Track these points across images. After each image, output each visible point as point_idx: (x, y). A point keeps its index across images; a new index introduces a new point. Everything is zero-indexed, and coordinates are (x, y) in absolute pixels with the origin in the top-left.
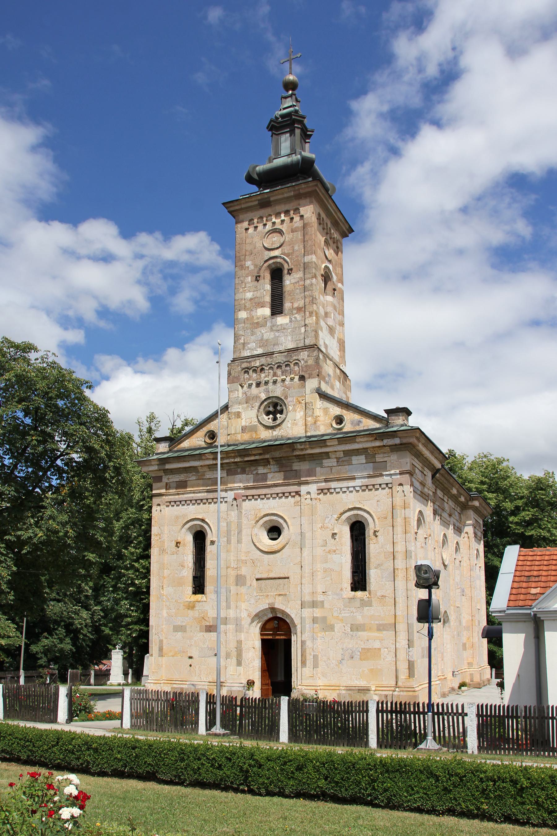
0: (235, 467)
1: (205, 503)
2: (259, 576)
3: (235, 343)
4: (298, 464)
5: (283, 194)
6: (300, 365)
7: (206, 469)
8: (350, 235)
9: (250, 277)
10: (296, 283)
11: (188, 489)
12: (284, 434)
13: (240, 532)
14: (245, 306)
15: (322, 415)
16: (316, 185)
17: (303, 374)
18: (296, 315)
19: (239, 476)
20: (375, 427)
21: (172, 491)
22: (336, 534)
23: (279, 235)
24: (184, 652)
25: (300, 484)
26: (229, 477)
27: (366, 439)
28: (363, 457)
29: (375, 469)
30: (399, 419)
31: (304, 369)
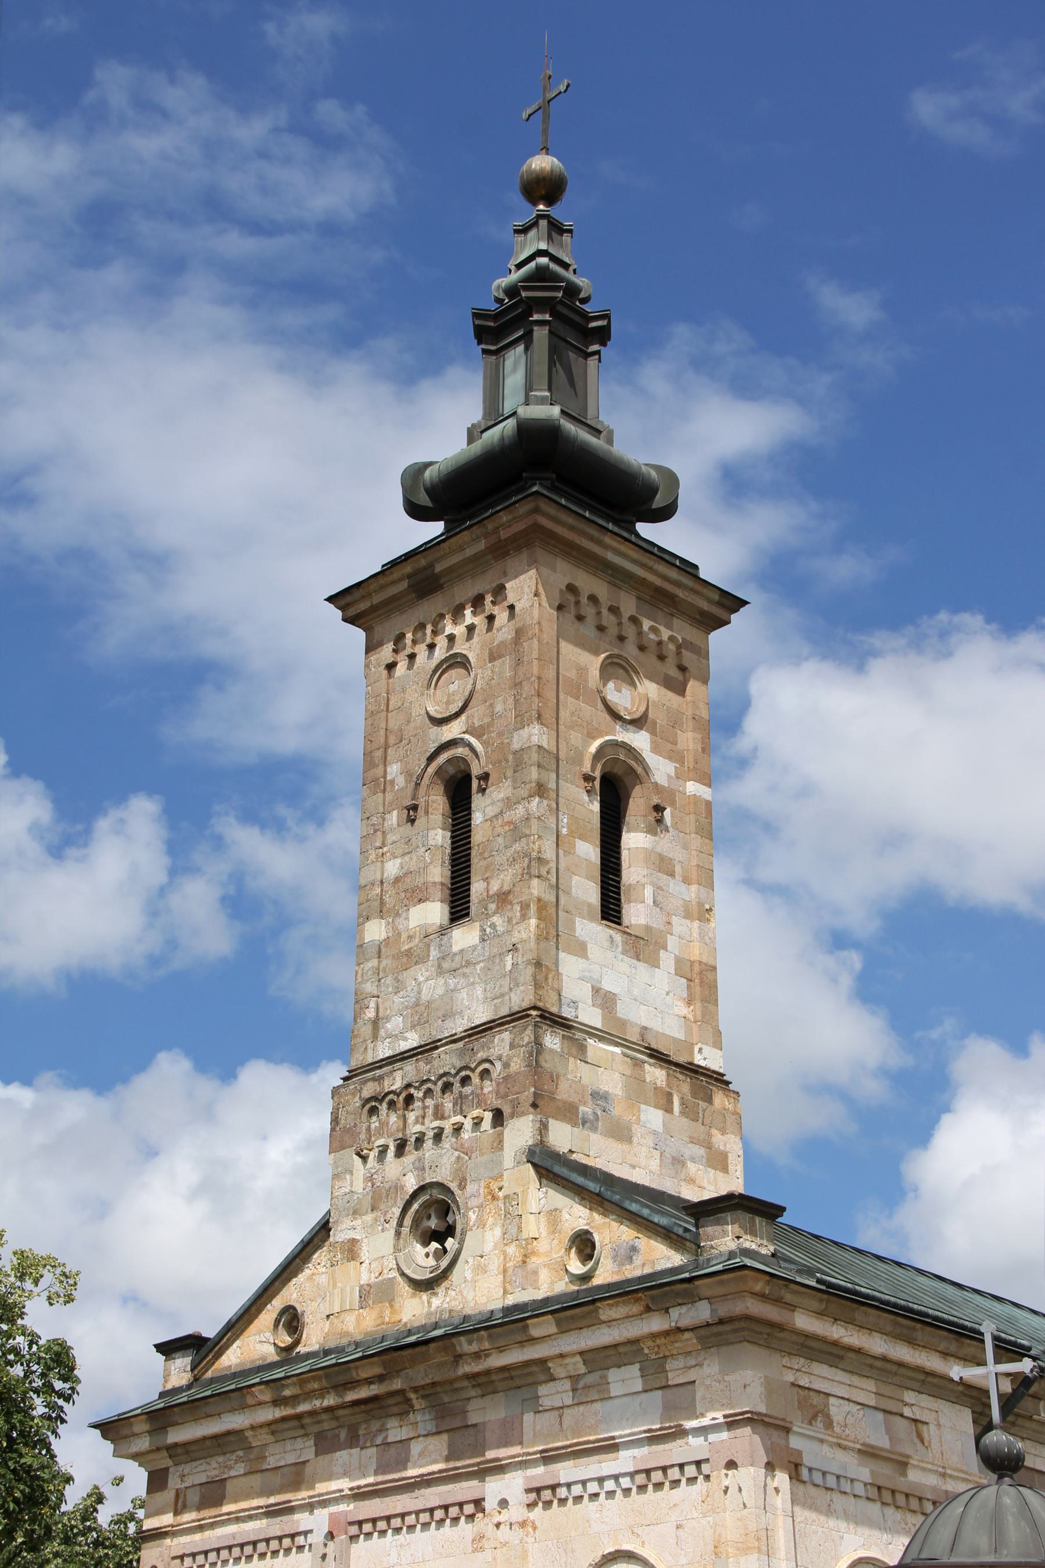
0: (334, 1424)
5: (461, 549)
7: (264, 1437)
8: (734, 617)
11: (226, 1509)
12: (456, 1305)
15: (544, 1233)
16: (536, 510)
18: (496, 919)
19: (343, 1456)
20: (669, 1265)
21: (189, 1517)
23: (462, 671)
25: (483, 1473)
28: (634, 1370)
29: (669, 1409)
30: (725, 1234)
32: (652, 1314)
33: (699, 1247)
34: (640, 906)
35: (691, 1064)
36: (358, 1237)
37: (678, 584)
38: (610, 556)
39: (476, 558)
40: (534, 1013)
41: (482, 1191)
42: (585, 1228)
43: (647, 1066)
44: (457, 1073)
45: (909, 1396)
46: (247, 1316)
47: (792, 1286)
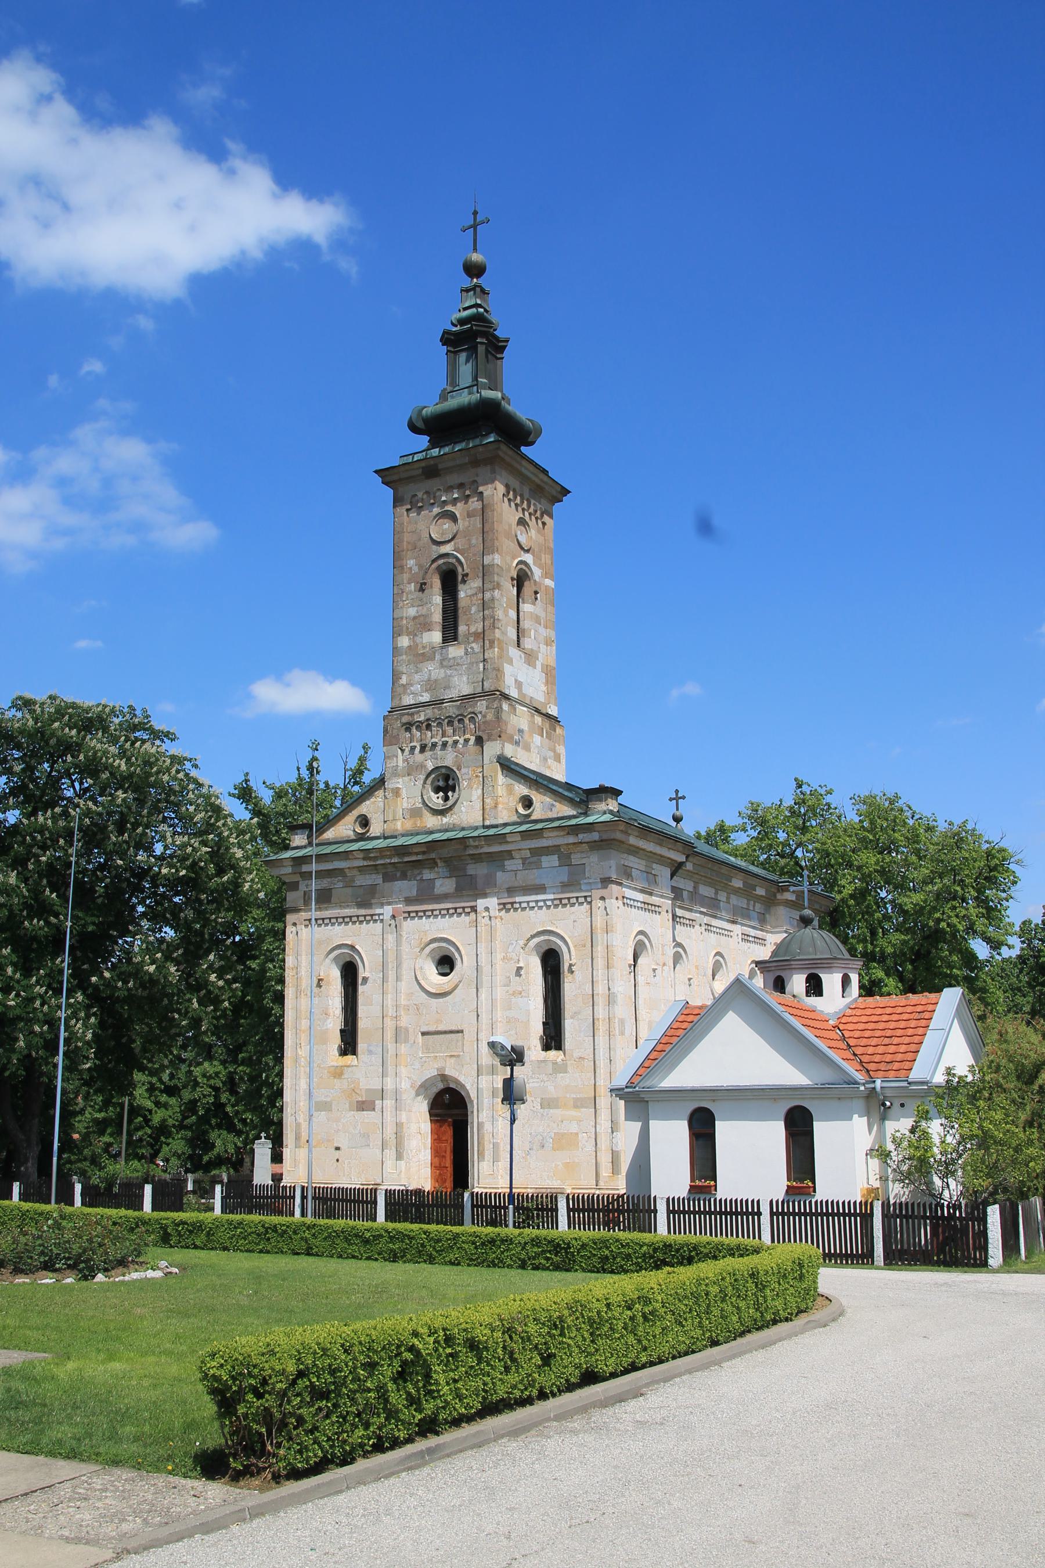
1: (354, 923)
2: (425, 1029)
4: (473, 866)
7: (355, 872)
13: (399, 966)
17: (480, 734)
18: (473, 645)
22: (521, 968)
24: (329, 1141)
26: (387, 884)
27: (555, 833)
31: (482, 727)
37: (545, 483)
45: (654, 866)
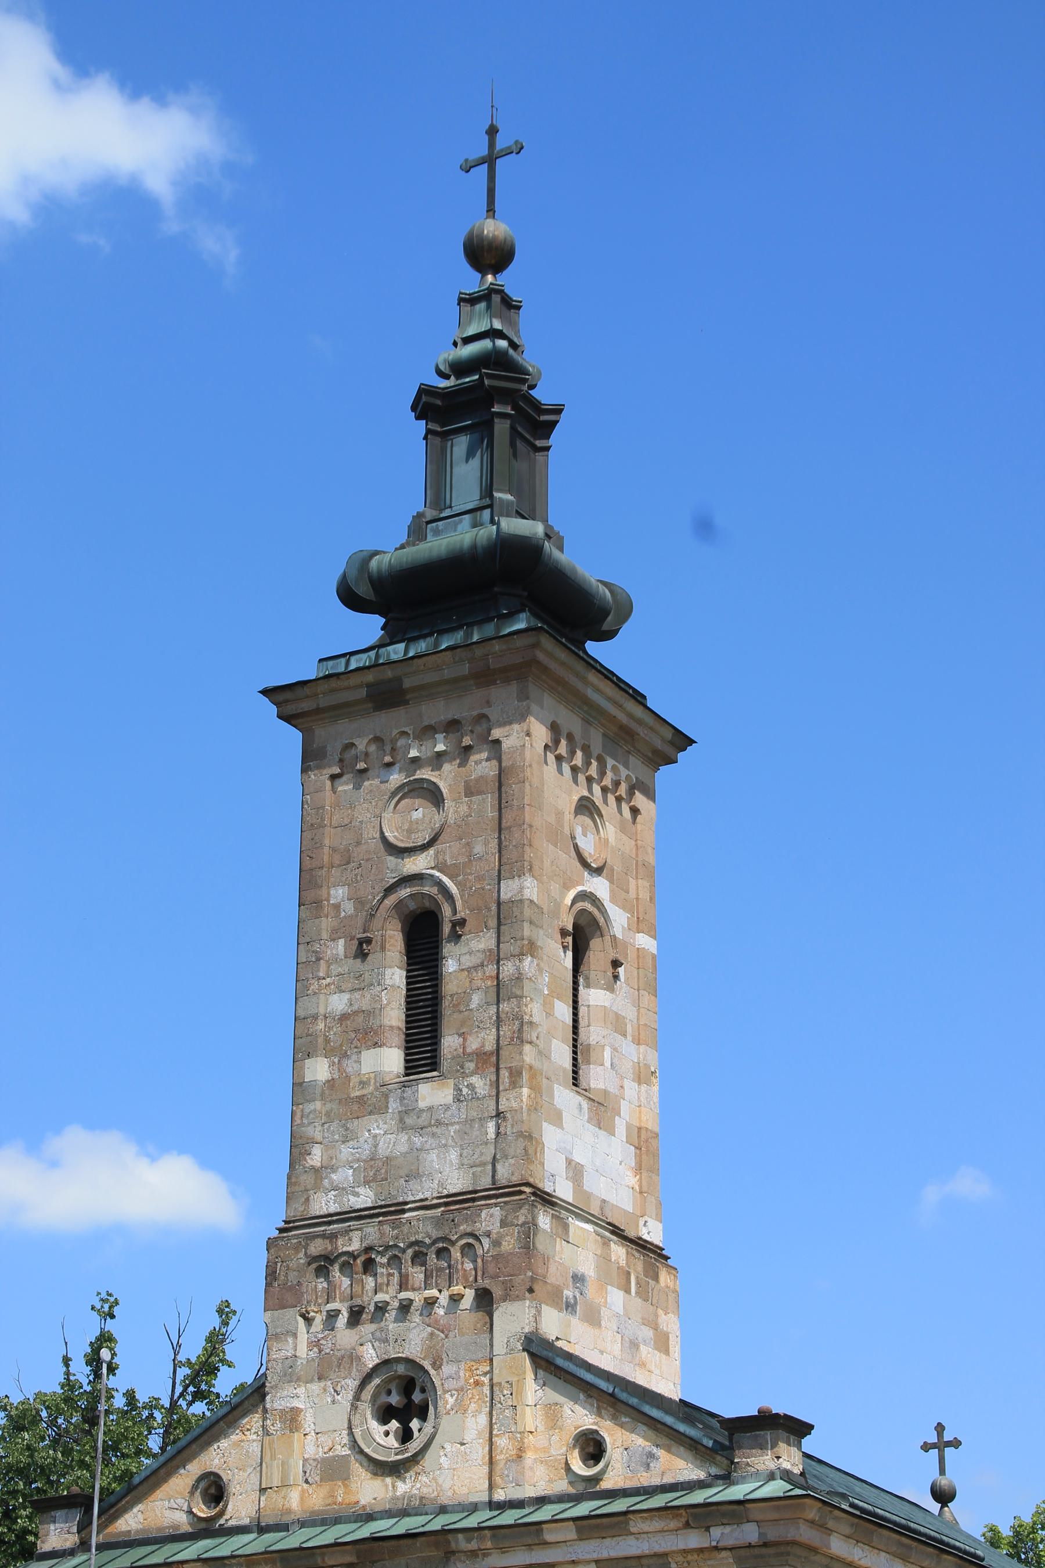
3: (292, 1165)
6: (480, 1252)
8: (681, 755)
9: (341, 942)
10: (475, 968)
12: (428, 1491)
14: (327, 1041)
18: (475, 1080)
27: (656, 1524)
31: (492, 1268)
32: (690, 1530)
33: (732, 1462)
34: (599, 1069)
35: (640, 1238)
36: (301, 1406)
38: (590, 693)
39: (454, 681)
40: (528, 1190)
41: (462, 1374)
42: (595, 1427)
43: (612, 1244)
44: (434, 1242)
46: (153, 1479)
47: (837, 1512)
